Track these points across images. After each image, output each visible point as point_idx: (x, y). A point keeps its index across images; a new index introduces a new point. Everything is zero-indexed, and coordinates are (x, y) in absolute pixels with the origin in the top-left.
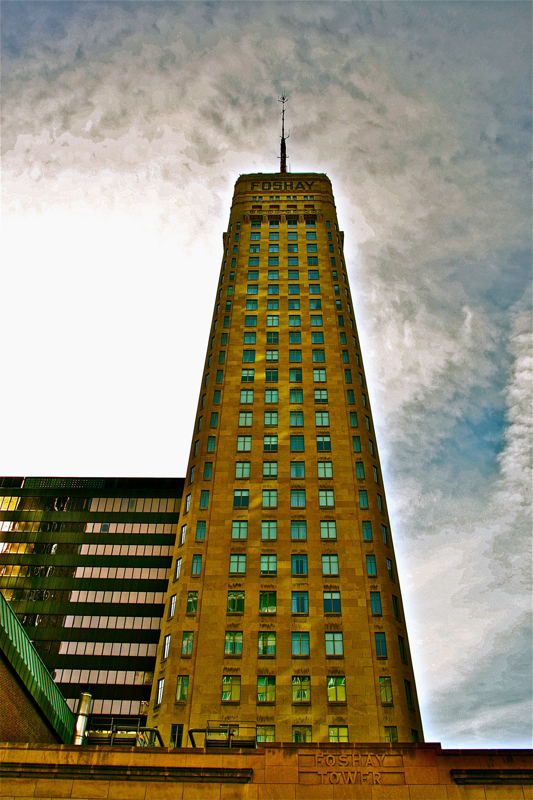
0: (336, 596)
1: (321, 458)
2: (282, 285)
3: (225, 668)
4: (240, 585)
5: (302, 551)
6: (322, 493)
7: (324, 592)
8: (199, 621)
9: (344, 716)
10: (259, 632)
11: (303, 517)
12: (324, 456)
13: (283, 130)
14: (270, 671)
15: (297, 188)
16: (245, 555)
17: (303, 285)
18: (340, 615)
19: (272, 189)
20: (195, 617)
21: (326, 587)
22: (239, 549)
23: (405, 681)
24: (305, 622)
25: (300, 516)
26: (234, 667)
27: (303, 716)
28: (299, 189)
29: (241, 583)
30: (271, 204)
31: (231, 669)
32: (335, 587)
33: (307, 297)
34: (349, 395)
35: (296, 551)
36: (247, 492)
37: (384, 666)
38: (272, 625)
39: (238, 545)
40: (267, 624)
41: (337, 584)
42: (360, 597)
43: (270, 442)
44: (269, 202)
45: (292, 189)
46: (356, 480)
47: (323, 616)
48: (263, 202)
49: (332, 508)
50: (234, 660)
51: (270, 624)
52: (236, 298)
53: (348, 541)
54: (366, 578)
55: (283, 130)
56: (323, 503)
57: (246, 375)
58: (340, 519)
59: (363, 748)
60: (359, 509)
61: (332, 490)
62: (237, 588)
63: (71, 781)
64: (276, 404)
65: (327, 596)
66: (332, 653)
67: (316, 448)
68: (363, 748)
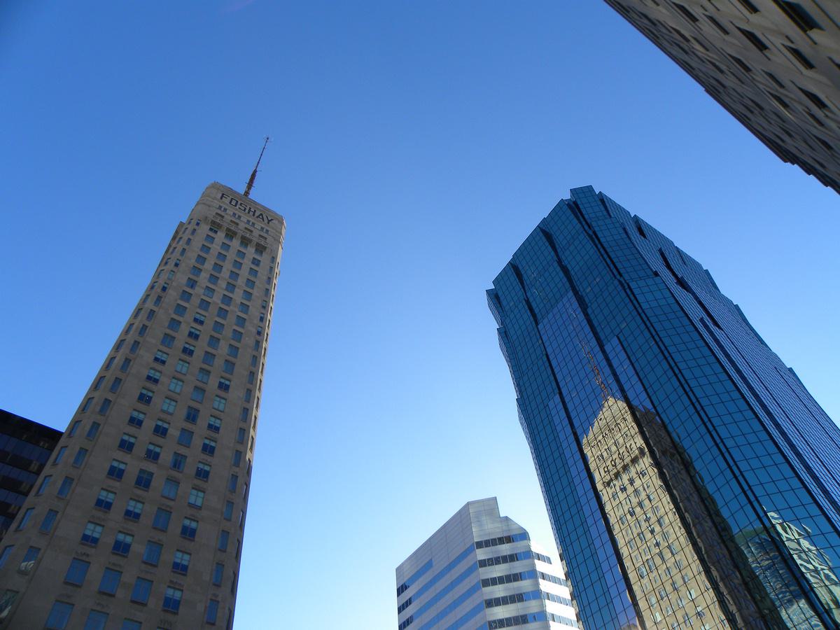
0: (178, 595)
1: (203, 459)
4: (88, 555)
5: (159, 540)
6: (194, 492)
7: (169, 587)
10: (92, 610)
11: (171, 508)
15: (258, 217)
16: (103, 526)
18: (177, 614)
20: (27, 577)
21: (171, 582)
25: (168, 506)
32: (180, 584)
34: (244, 411)
36: (125, 465)
43: (135, 507)
45: (254, 215)
49: (200, 508)
52: (174, 284)
56: (192, 500)
57: (103, 499)
61: (204, 492)
62: (84, 558)
64: (179, 394)
65: (170, 592)
66: (193, 503)
67: (201, 448)
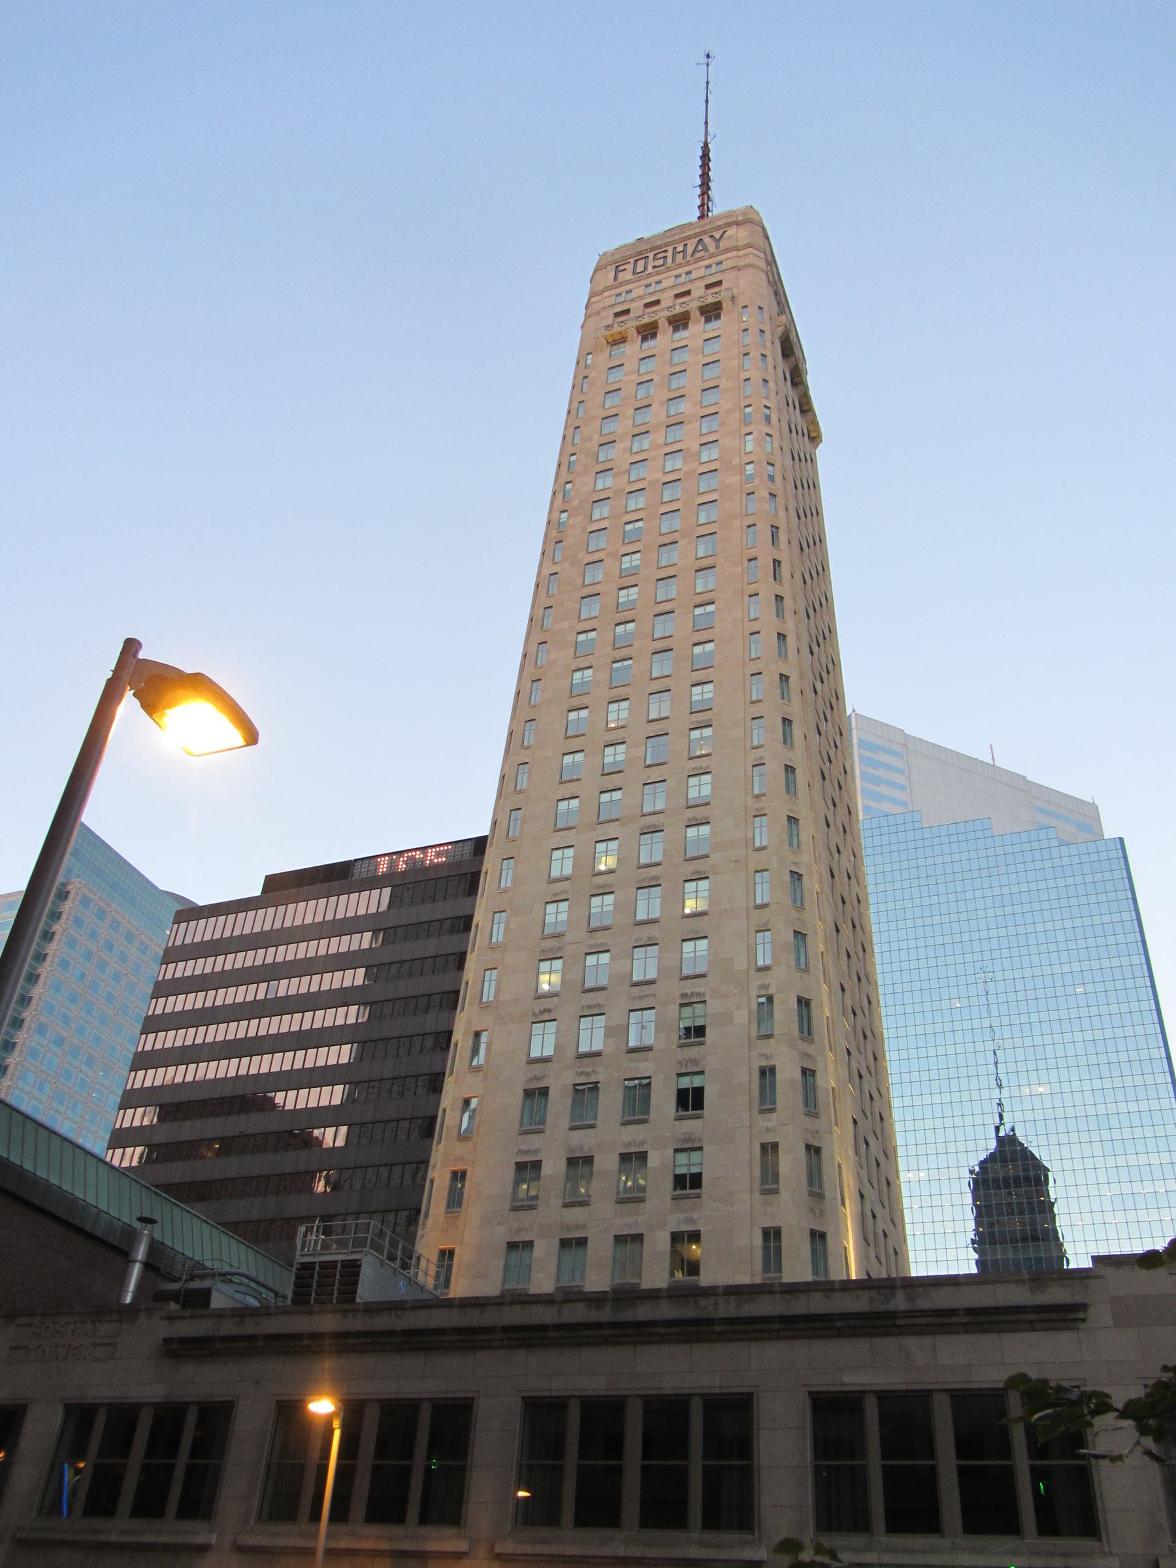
1: (694, 769)
2: (654, 459)
3: (520, 1151)
4: (550, 1010)
5: (650, 939)
8: (485, 1079)
9: (695, 1215)
11: (656, 878)
12: (698, 765)
13: (706, 123)
14: (586, 1149)
17: (689, 449)
19: (650, 270)
22: (552, 950)
23: (808, 1147)
24: (646, 1060)
26: (533, 1148)
27: (630, 1220)
28: (698, 255)
29: (552, 1006)
30: (647, 301)
31: (527, 1152)
33: (694, 471)
35: (641, 939)
37: (769, 1124)
38: (594, 1071)
39: (553, 943)
40: (586, 1070)
41: (701, 990)
42: (738, 1008)
44: (641, 297)
46: (749, 797)
47: (675, 1046)
48: (632, 300)
50: (532, 1136)
51: (590, 1070)
53: (726, 911)
54: (752, 972)
55: (706, 123)
58: (716, 873)
59: (259, 1283)
60: (750, 850)
63: (688, 1345)
68: (259, 1283)
